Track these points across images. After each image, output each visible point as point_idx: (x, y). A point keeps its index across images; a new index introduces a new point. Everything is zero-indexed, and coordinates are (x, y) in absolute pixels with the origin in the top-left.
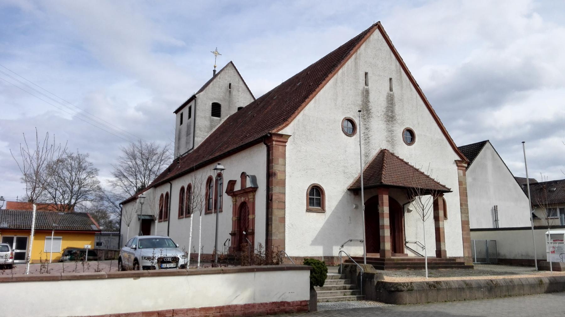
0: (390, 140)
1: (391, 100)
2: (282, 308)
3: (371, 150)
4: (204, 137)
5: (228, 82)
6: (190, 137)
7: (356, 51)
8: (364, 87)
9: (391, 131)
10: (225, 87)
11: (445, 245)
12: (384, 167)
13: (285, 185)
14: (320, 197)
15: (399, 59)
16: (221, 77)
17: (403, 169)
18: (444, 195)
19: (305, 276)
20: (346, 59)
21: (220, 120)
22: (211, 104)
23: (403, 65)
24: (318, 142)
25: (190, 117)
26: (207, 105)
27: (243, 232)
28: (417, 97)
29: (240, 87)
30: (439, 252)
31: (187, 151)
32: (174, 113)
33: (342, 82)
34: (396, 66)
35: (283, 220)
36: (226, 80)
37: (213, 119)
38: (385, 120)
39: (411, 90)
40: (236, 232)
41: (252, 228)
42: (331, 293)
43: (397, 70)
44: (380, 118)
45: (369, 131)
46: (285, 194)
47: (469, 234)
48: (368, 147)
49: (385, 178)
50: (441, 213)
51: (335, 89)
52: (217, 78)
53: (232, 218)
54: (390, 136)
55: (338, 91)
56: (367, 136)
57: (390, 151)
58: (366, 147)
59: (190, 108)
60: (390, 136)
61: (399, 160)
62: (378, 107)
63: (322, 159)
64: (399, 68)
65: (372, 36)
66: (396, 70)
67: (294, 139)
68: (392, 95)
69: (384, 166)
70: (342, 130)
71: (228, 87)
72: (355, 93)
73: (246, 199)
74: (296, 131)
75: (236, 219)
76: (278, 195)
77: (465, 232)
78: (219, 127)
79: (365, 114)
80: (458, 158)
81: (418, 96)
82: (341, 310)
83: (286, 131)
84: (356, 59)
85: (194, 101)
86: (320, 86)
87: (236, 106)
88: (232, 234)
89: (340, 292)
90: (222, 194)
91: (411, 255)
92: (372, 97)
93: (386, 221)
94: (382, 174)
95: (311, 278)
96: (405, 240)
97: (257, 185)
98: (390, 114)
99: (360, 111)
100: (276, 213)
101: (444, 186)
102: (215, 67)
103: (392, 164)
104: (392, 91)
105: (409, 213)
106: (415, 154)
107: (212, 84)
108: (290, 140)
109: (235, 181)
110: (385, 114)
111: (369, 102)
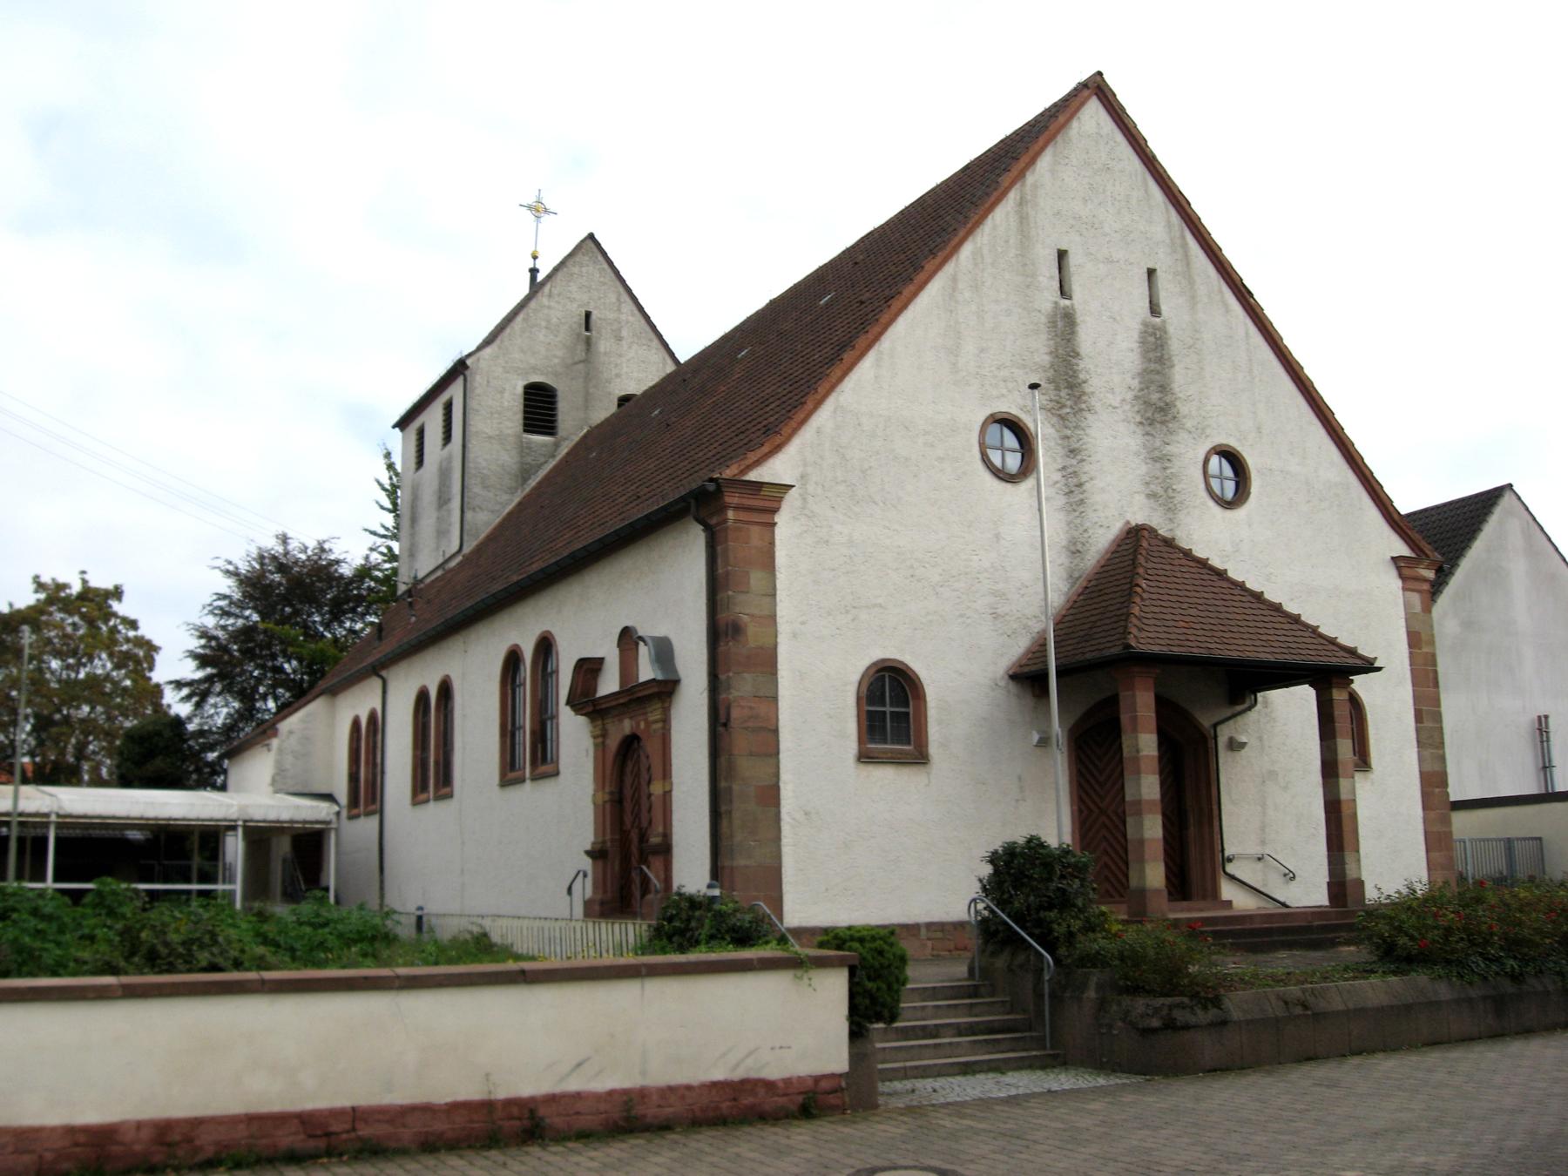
0: (1160, 491)
1: (1155, 346)
2: (747, 1100)
3: (1091, 532)
4: (497, 507)
5: (579, 306)
6: (449, 511)
7: (1021, 175)
8: (1056, 303)
9: (1160, 459)
10: (570, 327)
11: (1359, 860)
12: (1138, 589)
13: (776, 667)
14: (907, 705)
15: (1178, 202)
16: (555, 291)
17: (1206, 595)
18: (1352, 681)
19: (833, 988)
20: (987, 205)
21: (557, 445)
22: (520, 390)
23: (1193, 223)
24: (894, 506)
25: (447, 437)
26: (506, 395)
27: (82, 680)
28: (1247, 334)
29: (623, 324)
30: (1342, 886)
31: (441, 560)
32: (394, 427)
33: (976, 287)
34: (1169, 227)
35: (771, 795)
36: (572, 300)
37: (530, 442)
38: (1138, 419)
39: (1227, 310)
40: (609, 844)
41: (660, 829)
42: (936, 1046)
43: (1171, 240)
44: (1119, 411)
45: (1083, 460)
46: (774, 699)
47: (1447, 821)
48: (1078, 521)
49: (1140, 630)
50: (1345, 748)
51: (951, 311)
52: (542, 298)
53: (594, 795)
54: (1157, 478)
55: (961, 320)
56: (1075, 480)
57: (1160, 532)
58: (1071, 517)
59: (448, 407)
60: (1157, 478)
61: (1191, 564)
62: (1111, 373)
63: (912, 567)
64: (1178, 234)
65: (1075, 124)
66: (1168, 241)
67: (804, 500)
68: (1159, 329)
69: (1137, 585)
70: (983, 460)
71: (580, 324)
72: (1024, 324)
73: (638, 724)
74: (810, 470)
75: (607, 797)
76: (753, 705)
77: (1432, 814)
78: (551, 471)
79: (1063, 401)
80: (1402, 550)
81: (1253, 330)
82: (963, 1104)
83: (775, 470)
84: (1022, 203)
85: (460, 380)
86: (896, 304)
87: (610, 394)
88: (596, 854)
89: (970, 1042)
90: (557, 710)
91: (1242, 901)
92: (1088, 337)
93: (1148, 786)
94: (1129, 614)
95: (852, 996)
96: (1223, 850)
97: (675, 671)
98: (1155, 397)
99: (1034, 386)
100: (748, 769)
101: (1352, 652)
102: (535, 258)
103: (1168, 580)
104: (1160, 314)
105: (1236, 753)
106: (1252, 541)
107: (524, 319)
108: (790, 503)
109: (600, 661)
110: (1136, 398)
111: (1078, 354)
